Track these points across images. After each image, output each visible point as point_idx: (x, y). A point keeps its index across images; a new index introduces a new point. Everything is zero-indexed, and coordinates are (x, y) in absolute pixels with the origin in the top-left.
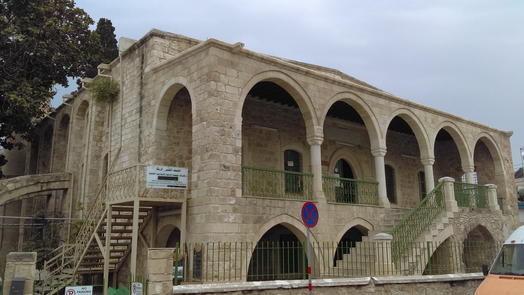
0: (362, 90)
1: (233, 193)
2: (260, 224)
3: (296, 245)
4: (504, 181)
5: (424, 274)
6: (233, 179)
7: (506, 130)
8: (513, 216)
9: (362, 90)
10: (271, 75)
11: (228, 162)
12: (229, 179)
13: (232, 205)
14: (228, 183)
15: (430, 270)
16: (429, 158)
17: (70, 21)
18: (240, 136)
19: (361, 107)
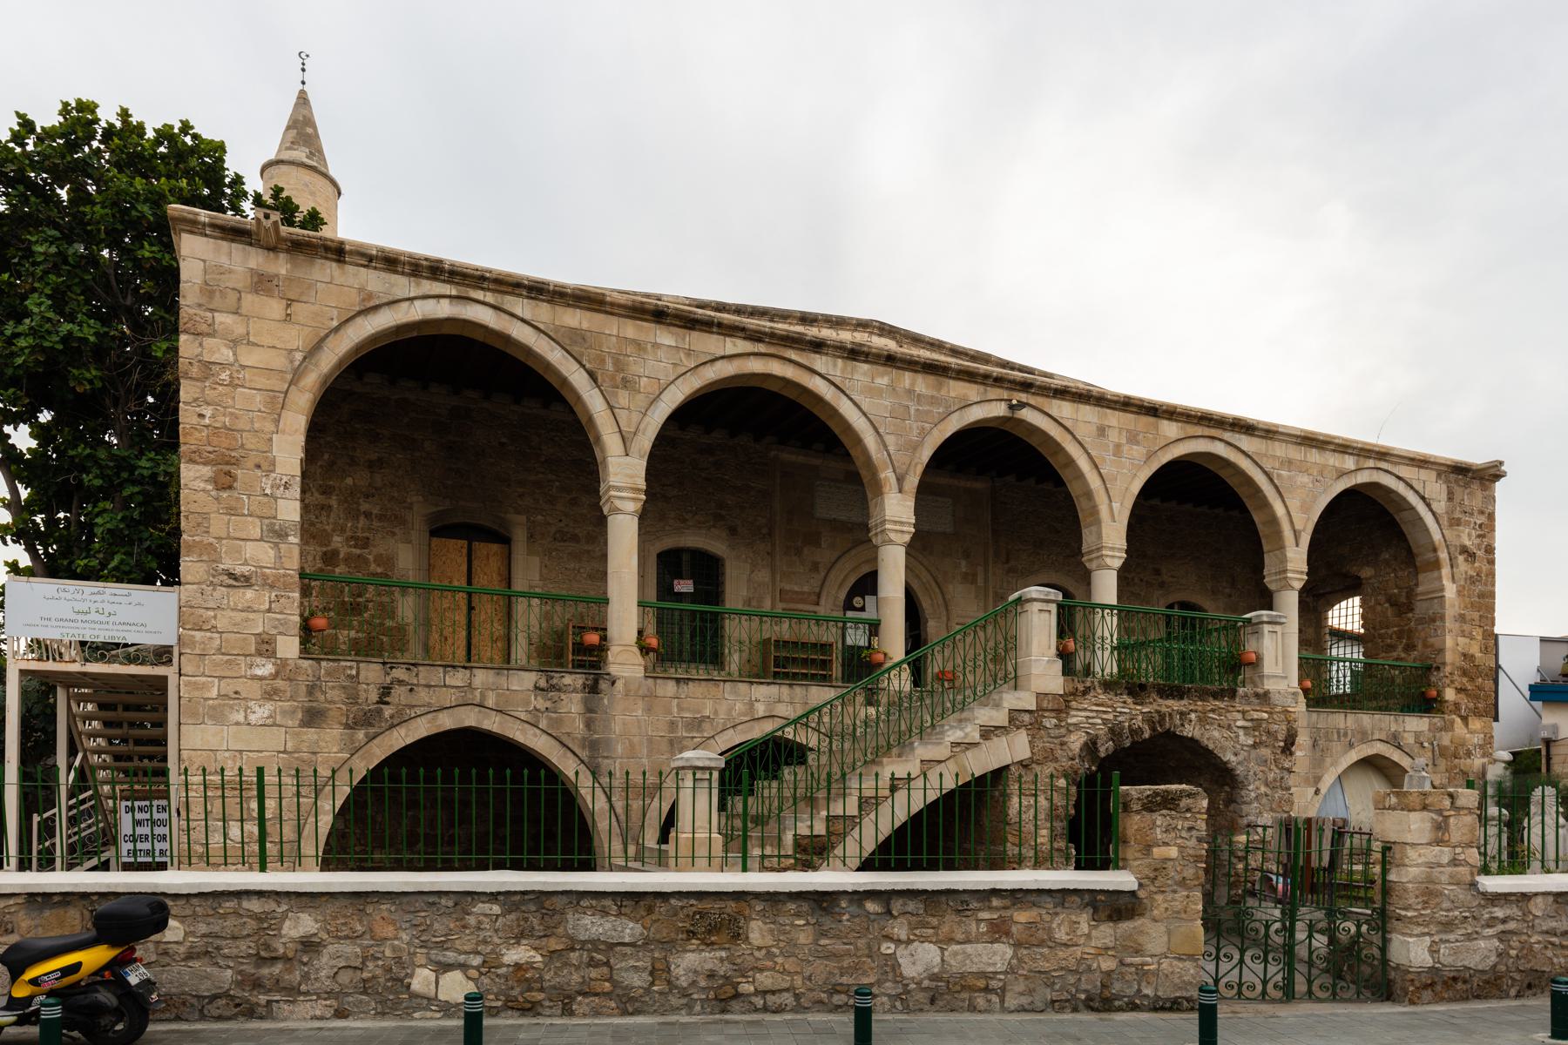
0: (1026, 386)
1: (266, 647)
2: (372, 731)
3: (534, 779)
4: (1442, 618)
5: (866, 866)
6: (277, 615)
7: (1476, 457)
8: (1465, 719)
9: (1026, 386)
10: (432, 306)
11: (246, 563)
12: (248, 609)
13: (261, 678)
14: (247, 620)
15: (901, 850)
16: (1099, 549)
17: (94, 260)
18: (296, 491)
19: (1058, 448)
